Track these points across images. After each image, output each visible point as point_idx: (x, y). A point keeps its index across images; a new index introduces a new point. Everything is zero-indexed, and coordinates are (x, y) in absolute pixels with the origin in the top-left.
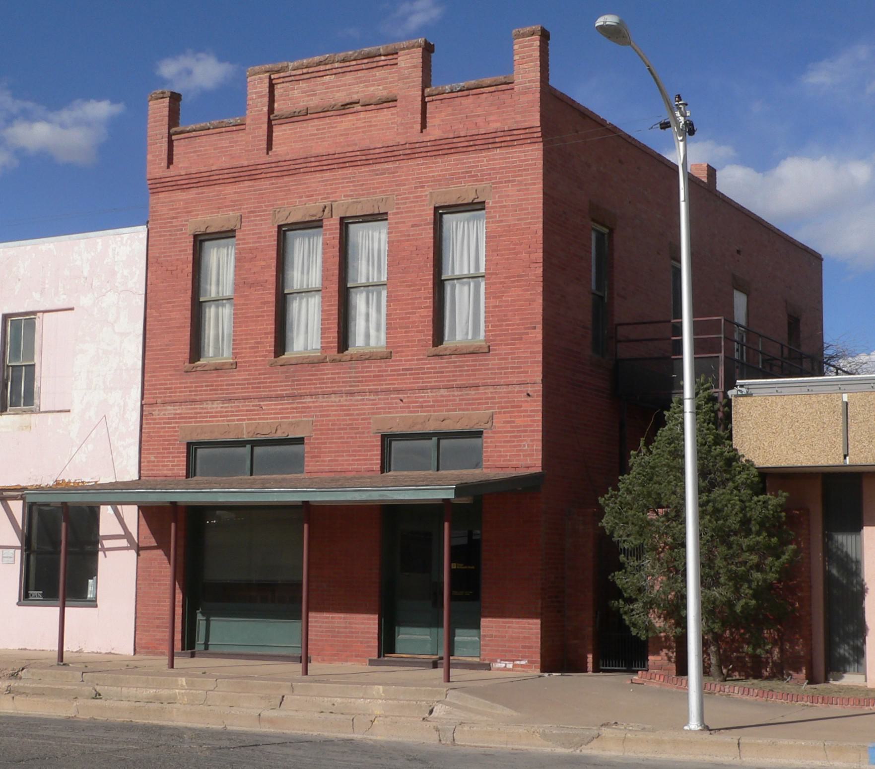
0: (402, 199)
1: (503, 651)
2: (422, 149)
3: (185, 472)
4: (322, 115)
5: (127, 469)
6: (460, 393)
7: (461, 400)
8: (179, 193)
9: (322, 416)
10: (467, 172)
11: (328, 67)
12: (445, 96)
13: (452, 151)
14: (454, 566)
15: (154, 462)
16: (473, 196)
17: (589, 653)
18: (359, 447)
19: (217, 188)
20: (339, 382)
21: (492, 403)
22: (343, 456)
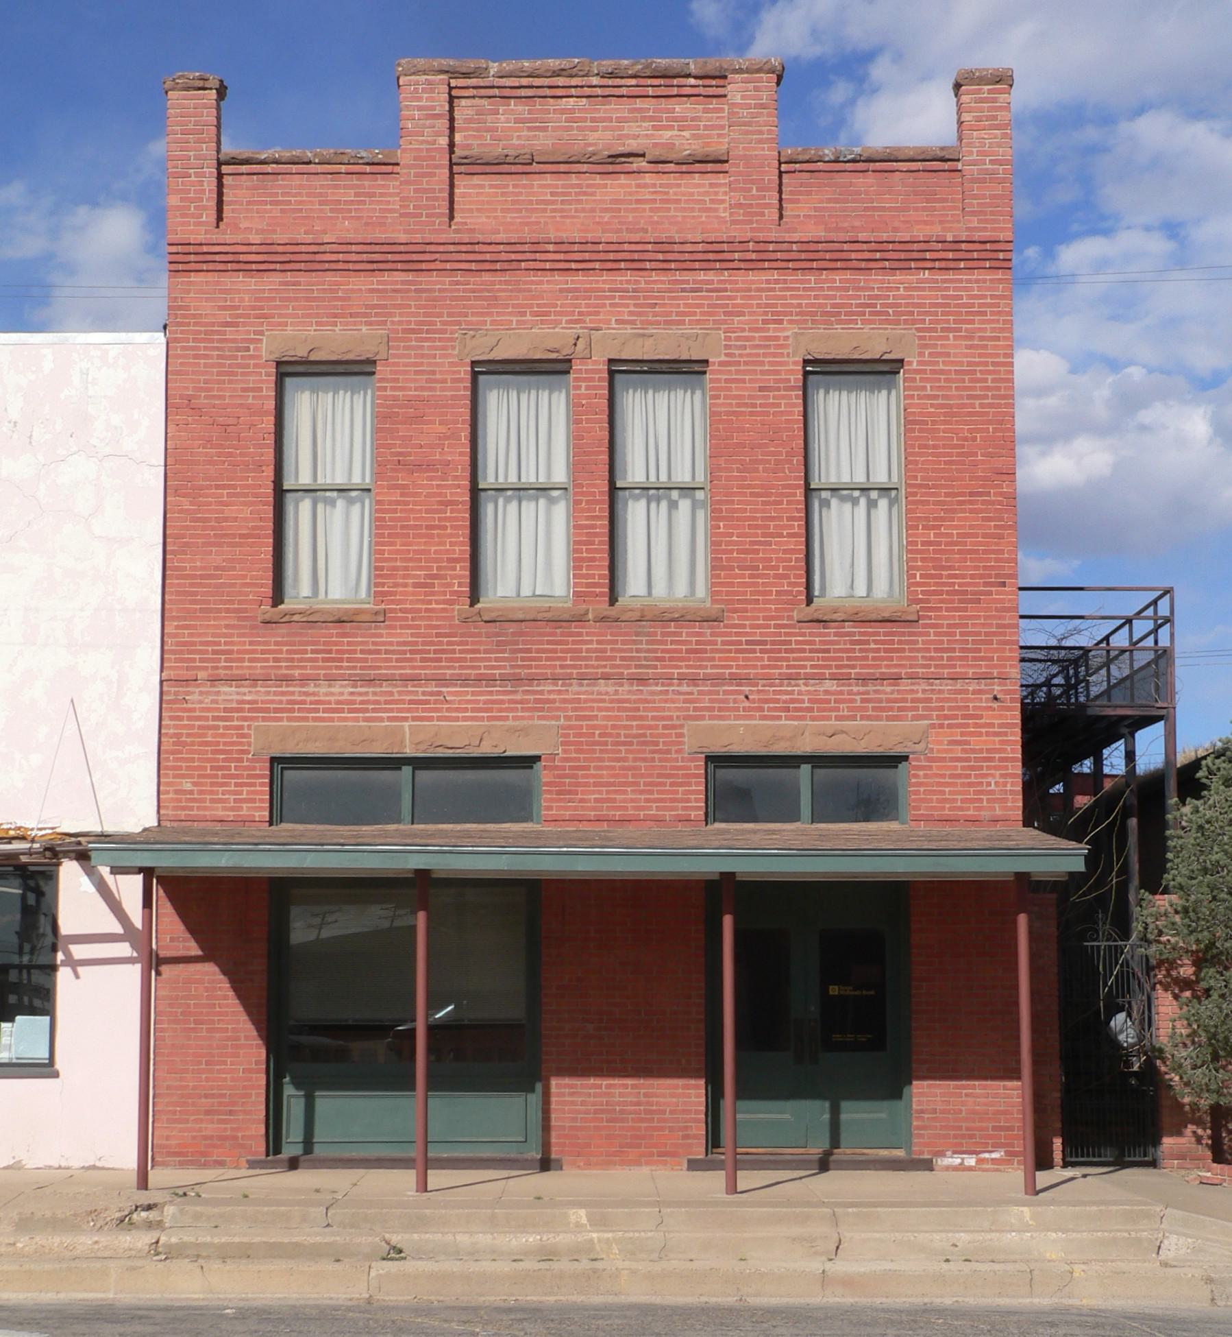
0: (738, 339)
1: (955, 1137)
2: (779, 255)
3: (267, 813)
4: (562, 168)
5: (130, 803)
6: (861, 689)
7: (863, 701)
8: (241, 277)
9: (579, 718)
10: (869, 305)
11: (574, 81)
12: (820, 165)
13: (839, 264)
14: (162, 993)
15: (191, 792)
16: (884, 348)
17: (1056, 1135)
18: (659, 776)
19: (330, 277)
20: (614, 658)
21: (924, 709)
22: (625, 792)
